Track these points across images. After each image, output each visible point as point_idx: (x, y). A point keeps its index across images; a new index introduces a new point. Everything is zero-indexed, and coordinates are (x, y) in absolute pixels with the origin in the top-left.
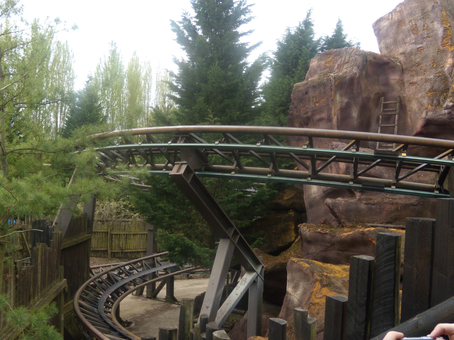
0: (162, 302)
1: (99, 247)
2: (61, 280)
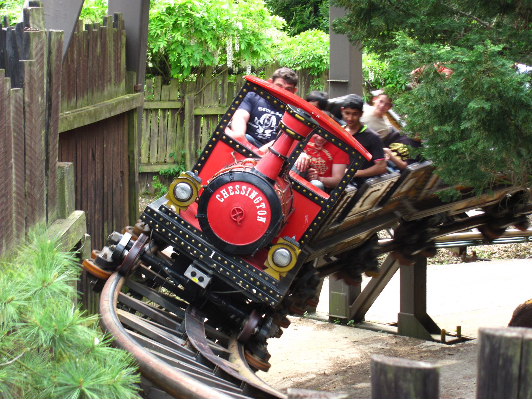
0: (385, 335)
1: (153, 160)
2: (63, 215)
